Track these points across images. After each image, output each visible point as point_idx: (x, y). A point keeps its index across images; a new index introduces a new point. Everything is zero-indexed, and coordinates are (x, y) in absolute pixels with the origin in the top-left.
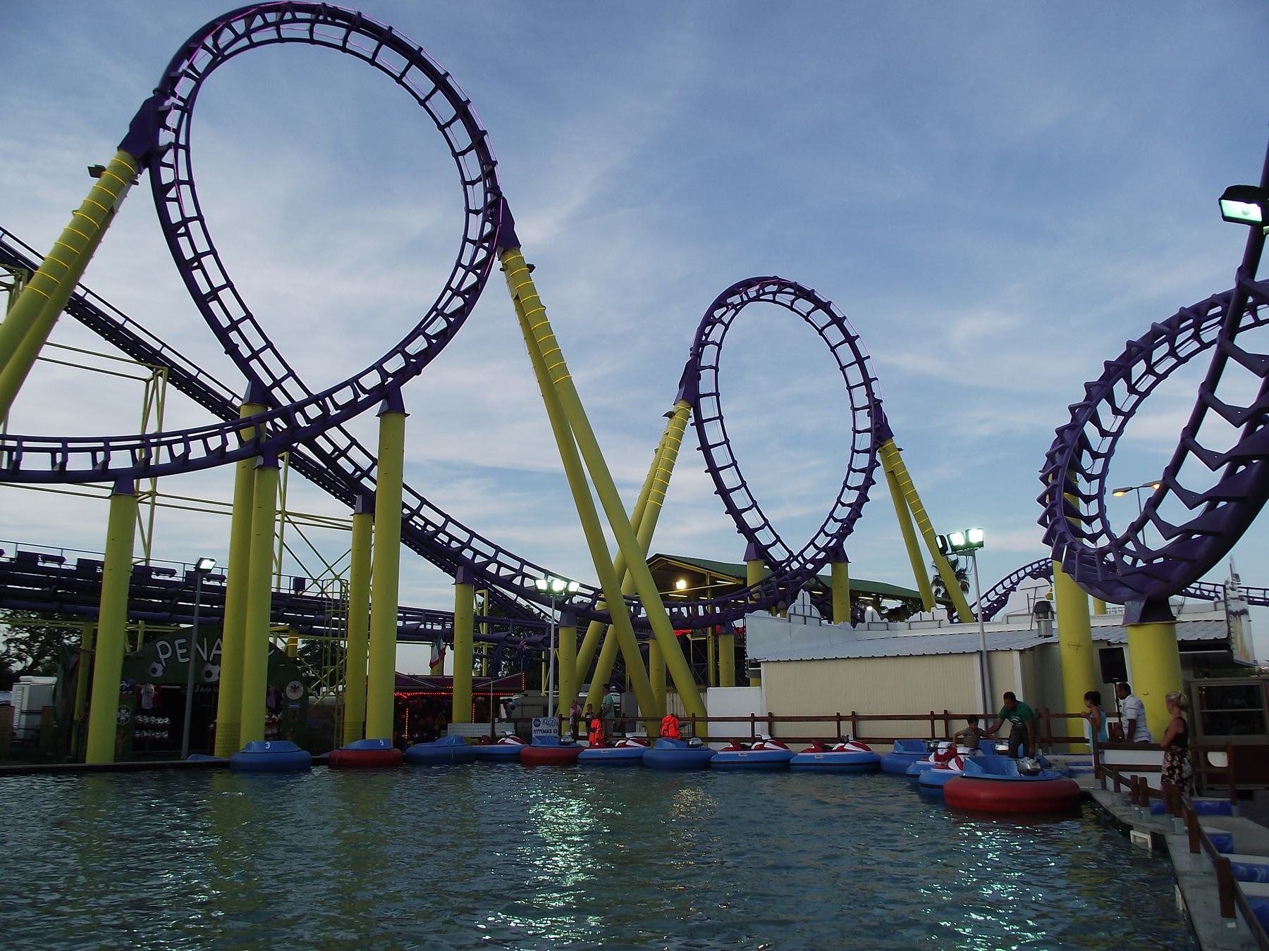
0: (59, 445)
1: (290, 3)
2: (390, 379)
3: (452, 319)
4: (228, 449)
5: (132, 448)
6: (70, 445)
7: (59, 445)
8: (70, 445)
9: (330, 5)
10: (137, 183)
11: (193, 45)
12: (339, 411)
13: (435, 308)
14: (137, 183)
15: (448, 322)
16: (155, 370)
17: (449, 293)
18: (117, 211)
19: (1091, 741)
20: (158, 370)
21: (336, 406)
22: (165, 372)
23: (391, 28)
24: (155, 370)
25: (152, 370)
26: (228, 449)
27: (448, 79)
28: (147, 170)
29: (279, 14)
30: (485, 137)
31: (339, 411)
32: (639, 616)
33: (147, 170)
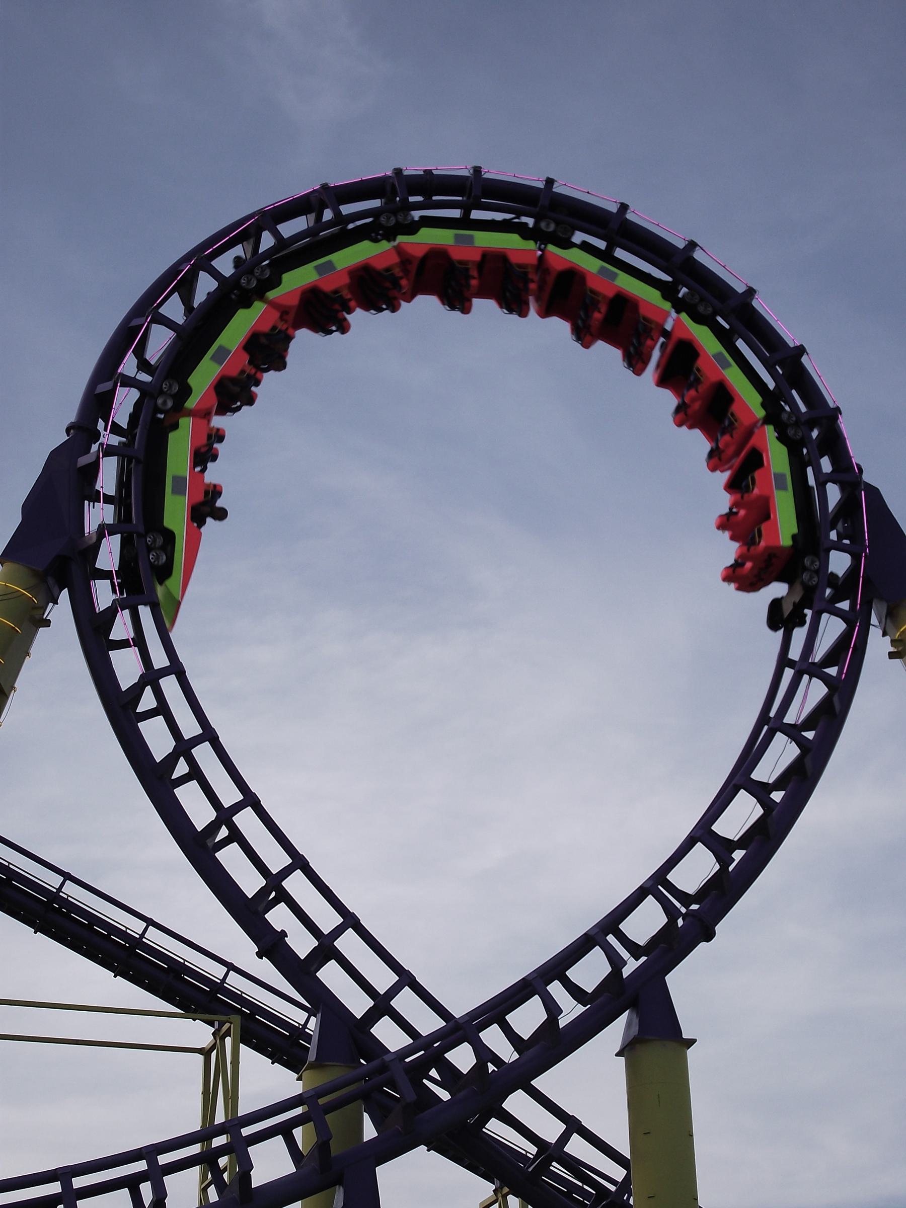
0: (141, 1166)
1: (325, 187)
2: (738, 855)
3: (810, 735)
4: (563, 1021)
5: (285, 1130)
6: (164, 1159)
7: (141, 1166)
8: (164, 1159)
9: (413, 167)
10: (47, 623)
11: (135, 322)
12: (644, 959)
13: (763, 718)
14: (47, 623)
15: (801, 743)
16: (216, 1024)
17: (789, 673)
18: (13, 688)
19: (315, 1040)
20: (221, 1024)
21: (634, 949)
22: (234, 1024)
23: (550, 182)
24: (216, 1024)
25: (212, 1025)
26: (563, 1021)
27: (698, 255)
28: (65, 592)
29: (312, 217)
30: (804, 360)
31: (644, 959)
32: (496, 1070)
33: (65, 595)
